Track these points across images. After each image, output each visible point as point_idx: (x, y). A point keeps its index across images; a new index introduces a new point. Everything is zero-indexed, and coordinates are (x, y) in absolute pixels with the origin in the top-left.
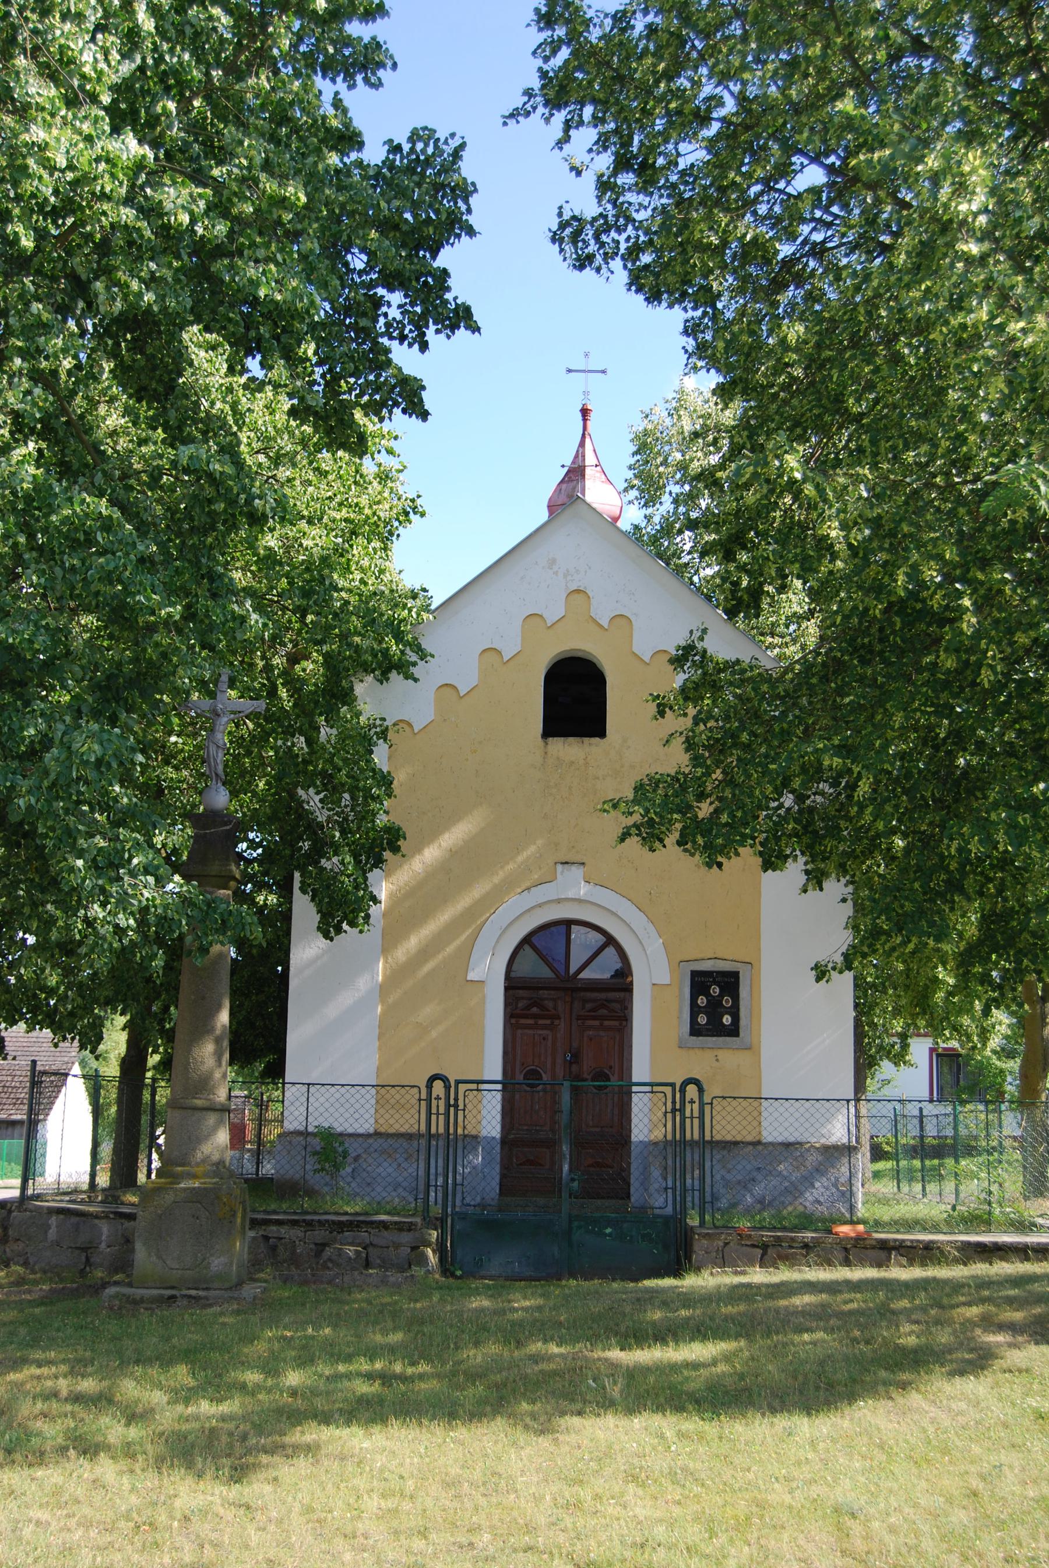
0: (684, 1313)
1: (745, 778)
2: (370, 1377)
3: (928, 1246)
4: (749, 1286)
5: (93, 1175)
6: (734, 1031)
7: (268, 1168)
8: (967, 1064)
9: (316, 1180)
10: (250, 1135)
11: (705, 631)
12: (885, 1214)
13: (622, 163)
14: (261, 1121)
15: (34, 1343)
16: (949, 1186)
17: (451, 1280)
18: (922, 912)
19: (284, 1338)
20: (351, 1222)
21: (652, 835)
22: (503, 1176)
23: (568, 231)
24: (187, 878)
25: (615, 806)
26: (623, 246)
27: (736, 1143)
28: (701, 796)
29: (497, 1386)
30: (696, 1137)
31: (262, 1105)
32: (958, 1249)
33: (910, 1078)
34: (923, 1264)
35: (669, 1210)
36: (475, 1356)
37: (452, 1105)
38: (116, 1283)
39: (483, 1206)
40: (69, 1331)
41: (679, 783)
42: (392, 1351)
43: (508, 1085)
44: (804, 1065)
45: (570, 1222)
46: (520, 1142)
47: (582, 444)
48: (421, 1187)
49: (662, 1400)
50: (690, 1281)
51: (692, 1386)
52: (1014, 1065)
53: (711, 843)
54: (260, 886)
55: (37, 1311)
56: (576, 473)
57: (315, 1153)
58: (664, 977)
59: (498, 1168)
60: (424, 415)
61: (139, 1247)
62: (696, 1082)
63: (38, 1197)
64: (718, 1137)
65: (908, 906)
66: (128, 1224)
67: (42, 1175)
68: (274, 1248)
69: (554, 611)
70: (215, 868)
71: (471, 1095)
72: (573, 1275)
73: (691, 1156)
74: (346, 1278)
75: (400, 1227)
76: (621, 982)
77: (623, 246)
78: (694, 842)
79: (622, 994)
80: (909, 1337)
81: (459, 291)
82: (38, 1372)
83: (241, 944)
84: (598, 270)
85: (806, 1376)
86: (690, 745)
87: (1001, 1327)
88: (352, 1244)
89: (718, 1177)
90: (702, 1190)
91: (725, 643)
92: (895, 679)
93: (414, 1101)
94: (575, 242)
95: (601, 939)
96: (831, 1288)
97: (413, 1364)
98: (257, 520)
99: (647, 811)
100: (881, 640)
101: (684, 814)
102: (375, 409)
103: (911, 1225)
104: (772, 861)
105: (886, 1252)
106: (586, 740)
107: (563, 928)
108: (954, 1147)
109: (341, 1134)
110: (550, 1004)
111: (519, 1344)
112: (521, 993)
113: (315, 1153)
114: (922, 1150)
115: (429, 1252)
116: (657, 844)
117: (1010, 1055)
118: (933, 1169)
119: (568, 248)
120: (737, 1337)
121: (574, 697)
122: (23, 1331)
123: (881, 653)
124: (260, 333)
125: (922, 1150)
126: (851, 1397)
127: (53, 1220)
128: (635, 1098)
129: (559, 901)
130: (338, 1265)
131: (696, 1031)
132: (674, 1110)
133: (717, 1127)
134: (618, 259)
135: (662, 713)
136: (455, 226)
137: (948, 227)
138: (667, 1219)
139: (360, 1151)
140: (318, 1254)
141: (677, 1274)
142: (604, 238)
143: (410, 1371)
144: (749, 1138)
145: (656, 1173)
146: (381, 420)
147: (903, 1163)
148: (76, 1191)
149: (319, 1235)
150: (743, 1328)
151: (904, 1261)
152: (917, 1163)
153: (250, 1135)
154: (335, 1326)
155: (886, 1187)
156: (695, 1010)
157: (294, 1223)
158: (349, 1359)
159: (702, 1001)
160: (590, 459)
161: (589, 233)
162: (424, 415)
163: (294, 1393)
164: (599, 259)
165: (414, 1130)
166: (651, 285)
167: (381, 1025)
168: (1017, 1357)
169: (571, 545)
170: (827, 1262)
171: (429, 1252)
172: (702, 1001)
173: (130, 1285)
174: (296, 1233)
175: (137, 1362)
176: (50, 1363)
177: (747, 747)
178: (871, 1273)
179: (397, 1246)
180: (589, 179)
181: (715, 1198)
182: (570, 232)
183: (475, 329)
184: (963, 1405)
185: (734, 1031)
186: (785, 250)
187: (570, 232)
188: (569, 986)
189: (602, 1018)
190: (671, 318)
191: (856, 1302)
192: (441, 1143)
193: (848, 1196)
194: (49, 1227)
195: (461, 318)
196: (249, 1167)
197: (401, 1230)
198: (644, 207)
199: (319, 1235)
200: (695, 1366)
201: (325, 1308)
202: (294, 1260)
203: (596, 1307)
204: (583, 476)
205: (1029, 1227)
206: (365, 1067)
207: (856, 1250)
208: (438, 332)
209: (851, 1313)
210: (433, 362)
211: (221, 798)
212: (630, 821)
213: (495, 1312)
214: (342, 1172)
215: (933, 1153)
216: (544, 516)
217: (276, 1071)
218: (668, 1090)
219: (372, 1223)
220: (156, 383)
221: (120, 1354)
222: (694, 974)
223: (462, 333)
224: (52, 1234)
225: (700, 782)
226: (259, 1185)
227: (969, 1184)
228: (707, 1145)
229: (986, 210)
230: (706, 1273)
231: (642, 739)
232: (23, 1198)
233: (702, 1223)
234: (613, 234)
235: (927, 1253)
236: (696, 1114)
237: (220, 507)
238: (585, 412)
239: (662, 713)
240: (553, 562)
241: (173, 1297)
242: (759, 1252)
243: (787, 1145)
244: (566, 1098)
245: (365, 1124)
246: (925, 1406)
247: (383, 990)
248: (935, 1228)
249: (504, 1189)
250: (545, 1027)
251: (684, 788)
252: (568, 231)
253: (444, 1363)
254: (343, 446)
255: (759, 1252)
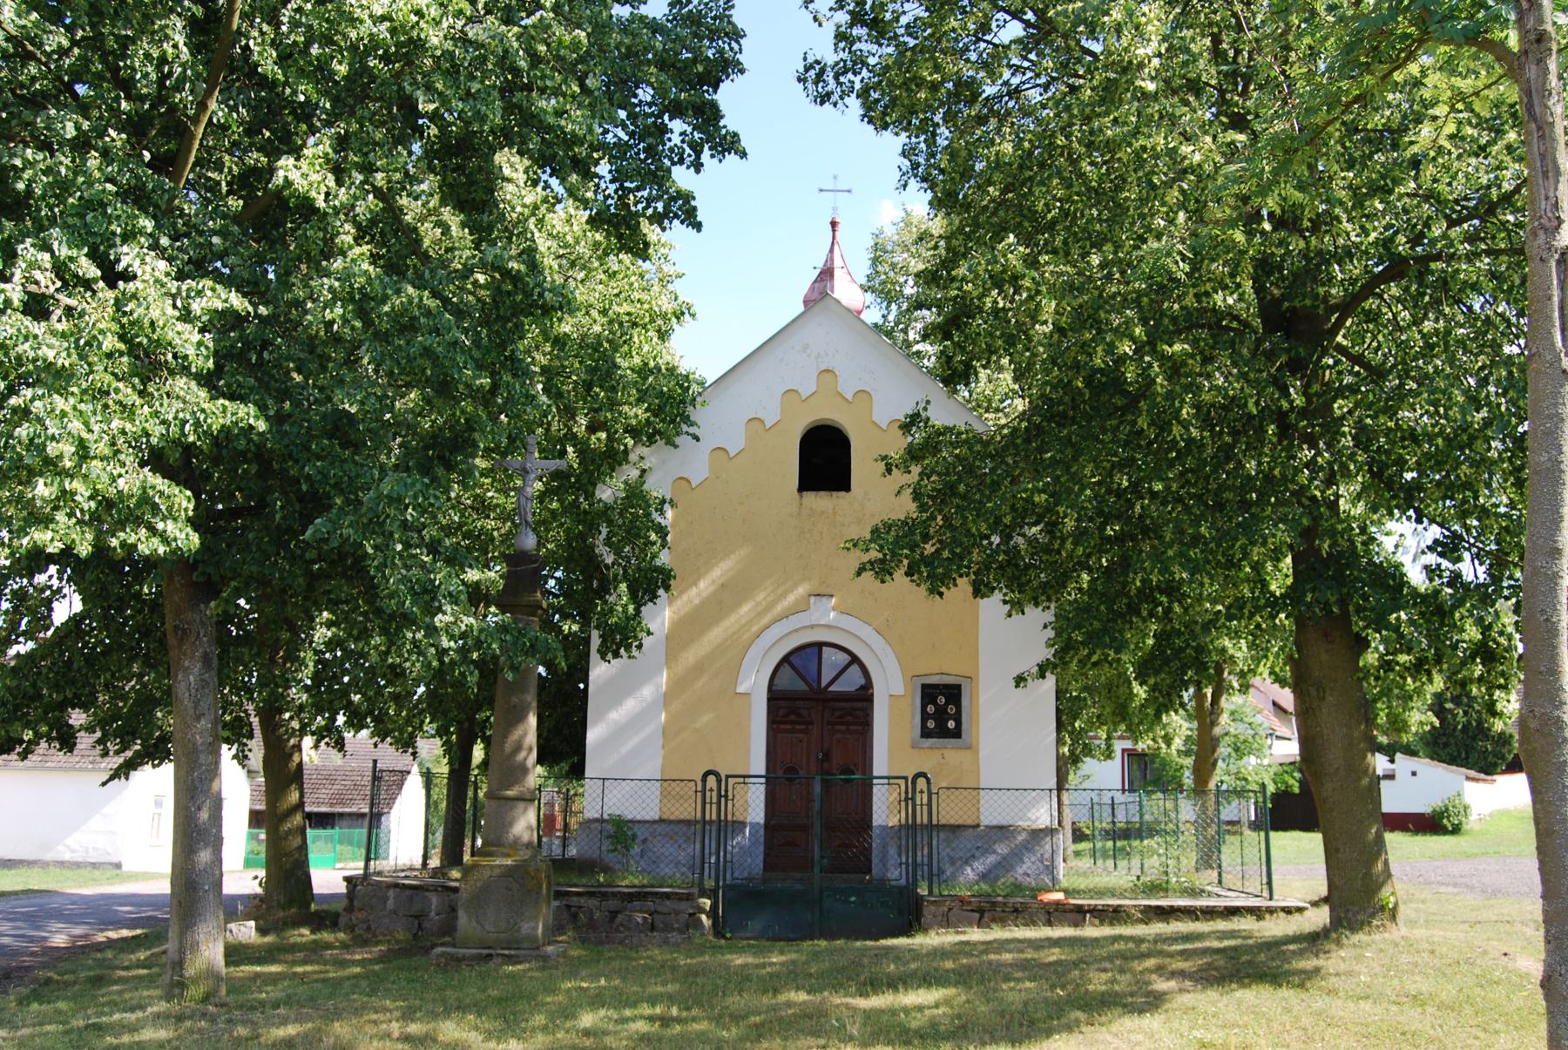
0: (913, 966)
1: (962, 522)
2: (651, 1019)
3: (1117, 910)
4: (967, 943)
5: (425, 857)
6: (957, 733)
7: (572, 851)
8: (1153, 762)
9: (610, 858)
10: (559, 824)
11: (928, 402)
12: (1082, 883)
13: (857, 18)
14: (566, 810)
15: (373, 992)
16: (1136, 862)
17: (723, 942)
18: (1105, 630)
19: (582, 988)
20: (639, 893)
21: (883, 570)
22: (766, 855)
23: (812, 73)
24: (503, 609)
25: (855, 545)
26: (858, 86)
27: (959, 826)
28: (926, 538)
29: (756, 1025)
30: (925, 821)
31: (568, 799)
32: (1141, 912)
33: (1103, 774)
34: (1111, 924)
35: (903, 882)
36: (735, 1001)
37: (723, 796)
38: (443, 945)
39: (750, 879)
40: (403, 983)
41: (908, 526)
42: (671, 999)
43: (771, 780)
44: (1014, 762)
45: (821, 891)
46: (781, 826)
47: (832, 251)
48: (698, 861)
49: (892, 1036)
50: (920, 941)
51: (914, 1024)
52: (1189, 761)
53: (936, 577)
54: (565, 617)
55: (377, 967)
56: (827, 274)
57: (609, 837)
58: (899, 688)
59: (762, 848)
60: (698, 226)
61: (461, 913)
62: (924, 775)
63: (379, 873)
64: (943, 821)
65: (1096, 624)
66: (453, 896)
67: (387, 858)
68: (575, 916)
69: (807, 387)
70: (527, 599)
71: (738, 787)
72: (822, 936)
73: (921, 839)
74: (635, 940)
75: (680, 898)
76: (864, 696)
77: (858, 86)
78: (920, 573)
79: (860, 705)
80: (1098, 982)
81: (730, 122)
82: (375, 1017)
83: (549, 666)
84: (835, 105)
85: (1012, 1015)
86: (917, 496)
87: (1173, 974)
88: (640, 911)
89: (943, 854)
90: (930, 865)
91: (945, 412)
92: (1085, 439)
93: (691, 793)
94: (816, 83)
95: (847, 658)
96: (1037, 945)
97: (688, 1009)
98: (547, 310)
99: (882, 547)
100: (1073, 409)
101: (912, 550)
102: (658, 219)
103: (1101, 893)
104: (980, 590)
105: (1078, 914)
106: (835, 494)
107: (816, 649)
108: (1139, 831)
109: (631, 821)
110: (805, 712)
111: (776, 991)
112: (782, 703)
113: (609, 837)
114: (1114, 834)
115: (704, 917)
116: (888, 578)
117: (1187, 753)
118: (1123, 849)
119: (810, 85)
120: (956, 984)
121: (824, 459)
122: (364, 984)
123: (1073, 419)
124: (561, 157)
125: (1114, 834)
126: (1049, 1033)
127: (391, 893)
128: (875, 789)
129: (812, 627)
130: (629, 929)
131: (926, 733)
132: (906, 799)
133: (943, 813)
134: (854, 96)
135: (889, 471)
136: (727, 66)
137: (1129, 69)
138: (901, 890)
139: (647, 834)
140: (612, 920)
141: (907, 931)
142: (842, 79)
143: (684, 1014)
144: (969, 822)
145: (892, 851)
146: (664, 229)
147: (1099, 845)
148: (411, 869)
149: (613, 904)
150: (962, 978)
151: (1097, 922)
152: (1110, 844)
153: (559, 824)
154: (624, 979)
155: (1085, 863)
156: (925, 717)
157: (591, 894)
158: (634, 1005)
159: (931, 709)
160: (838, 262)
161: (829, 77)
162: (698, 226)
163: (587, 1033)
164: (835, 97)
165: (690, 817)
166: (877, 116)
167: (662, 729)
168: (1187, 999)
169: (823, 335)
170: (1031, 922)
171: (704, 917)
172: (931, 709)
173: (454, 946)
174: (592, 903)
175: (458, 1008)
176: (385, 1010)
177: (964, 497)
178: (1067, 932)
179: (677, 913)
180: (829, 30)
181: (941, 872)
182: (813, 75)
183: (743, 155)
184: (1140, 1037)
185: (957, 733)
186: (989, 90)
187: (813, 75)
188: (820, 697)
189: (848, 724)
190: (892, 143)
191: (1054, 955)
192: (714, 828)
193: (1051, 869)
194: (388, 898)
195: (729, 145)
196: (557, 850)
197: (680, 899)
198: (877, 53)
199: (613, 904)
200: (920, 1008)
201: (616, 964)
202: (592, 925)
203: (843, 962)
204: (832, 276)
205: (1201, 893)
206: (652, 767)
207: (1055, 914)
208: (712, 156)
209: (1050, 964)
210: (708, 182)
211: (529, 541)
212: (866, 558)
213: (757, 966)
214: (632, 852)
215: (1125, 834)
216: (802, 309)
217: (578, 771)
218: (902, 782)
219: (657, 893)
220: (473, 195)
221: (444, 1001)
222: (924, 687)
223: (731, 158)
224: (390, 904)
225: (925, 524)
226: (562, 865)
227: (1150, 859)
228: (932, 828)
229: (1159, 55)
230: (932, 933)
231: (879, 494)
232: (366, 875)
233: (931, 893)
234: (850, 76)
235: (1114, 915)
236: (925, 801)
237: (521, 299)
238: (834, 224)
239: (889, 471)
240: (806, 347)
241: (490, 955)
242: (977, 915)
243: (1001, 828)
244: (817, 788)
245: (652, 814)
246: (1109, 1038)
247: (667, 698)
248: (1122, 896)
249: (769, 865)
250: (801, 731)
251: (911, 532)
252: (812, 73)
253: (713, 1008)
254: (629, 250)
255: (977, 915)
